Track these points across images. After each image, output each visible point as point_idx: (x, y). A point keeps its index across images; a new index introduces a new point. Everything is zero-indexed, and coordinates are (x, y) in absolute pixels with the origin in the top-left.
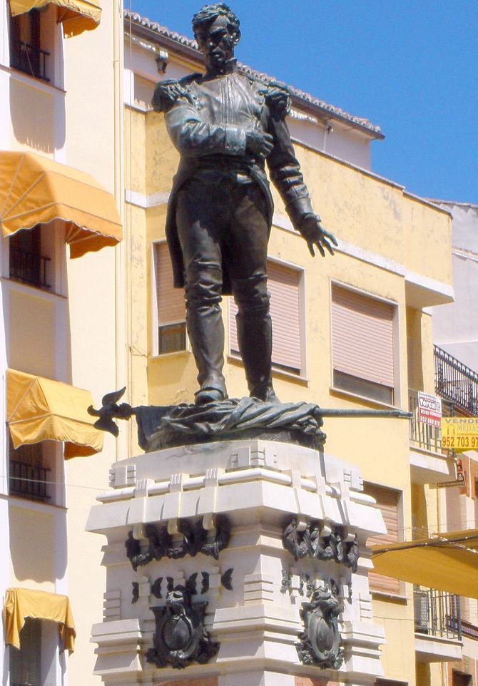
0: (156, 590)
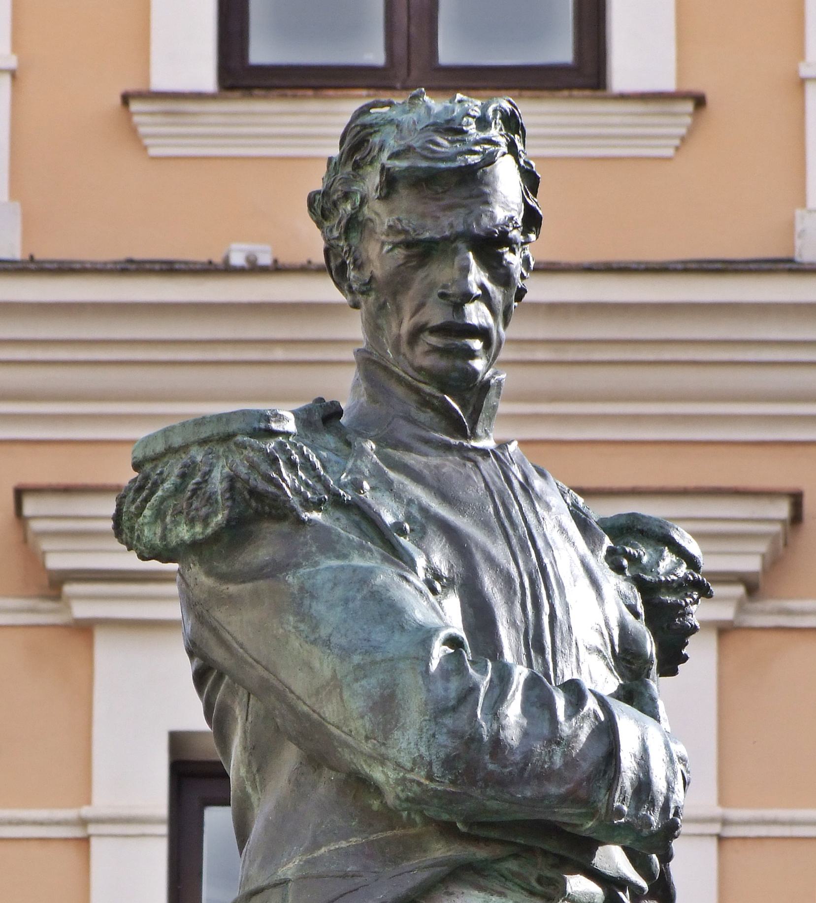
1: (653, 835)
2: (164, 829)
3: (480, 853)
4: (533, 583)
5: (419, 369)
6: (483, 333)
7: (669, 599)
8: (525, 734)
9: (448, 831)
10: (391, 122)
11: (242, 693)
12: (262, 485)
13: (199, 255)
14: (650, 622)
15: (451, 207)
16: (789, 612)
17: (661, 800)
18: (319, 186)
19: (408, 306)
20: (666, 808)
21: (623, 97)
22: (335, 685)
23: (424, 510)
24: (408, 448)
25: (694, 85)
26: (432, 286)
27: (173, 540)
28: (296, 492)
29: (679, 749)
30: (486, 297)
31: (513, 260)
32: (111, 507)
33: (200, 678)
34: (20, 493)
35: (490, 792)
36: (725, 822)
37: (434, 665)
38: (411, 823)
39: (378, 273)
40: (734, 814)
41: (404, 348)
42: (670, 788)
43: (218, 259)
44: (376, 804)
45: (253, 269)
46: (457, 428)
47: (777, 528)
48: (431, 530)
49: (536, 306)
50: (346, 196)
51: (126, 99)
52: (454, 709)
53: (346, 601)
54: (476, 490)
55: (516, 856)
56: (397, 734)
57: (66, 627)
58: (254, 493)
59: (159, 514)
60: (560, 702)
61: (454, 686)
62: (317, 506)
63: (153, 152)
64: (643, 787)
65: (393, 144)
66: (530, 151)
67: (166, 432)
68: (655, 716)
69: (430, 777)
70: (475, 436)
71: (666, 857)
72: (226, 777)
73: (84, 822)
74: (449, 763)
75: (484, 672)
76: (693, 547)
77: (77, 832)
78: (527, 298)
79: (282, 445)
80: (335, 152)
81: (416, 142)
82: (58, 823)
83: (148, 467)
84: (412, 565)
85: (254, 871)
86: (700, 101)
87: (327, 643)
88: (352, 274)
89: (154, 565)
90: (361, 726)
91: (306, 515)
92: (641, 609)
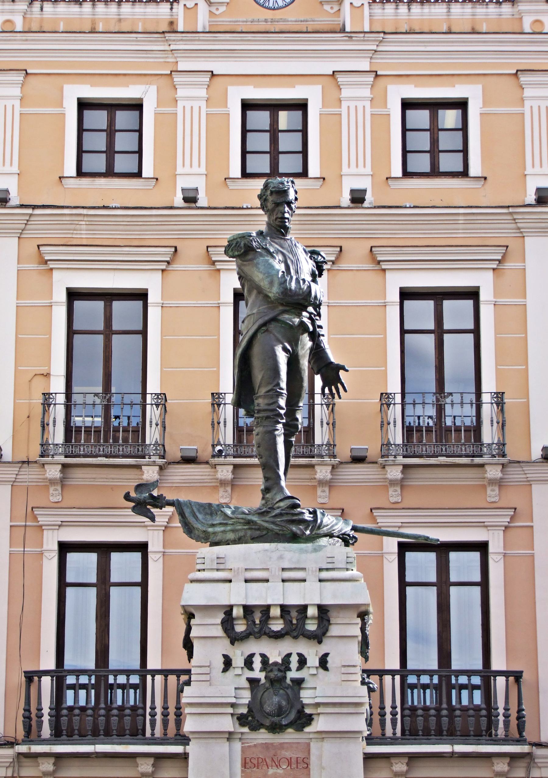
0: (249, 663)
1: (318, 305)
2: (233, 305)
3: (288, 308)
4: (297, 262)
5: (277, 225)
6: (288, 219)
7: (320, 264)
8: (295, 288)
9: (282, 305)
10: (272, 182)
11: (247, 281)
12: (250, 245)
13: (238, 206)
14: (317, 268)
15: (282, 197)
16: (340, 267)
17: (319, 299)
18: (259, 193)
19: (275, 214)
20: (320, 300)
21: (311, 178)
22: (263, 279)
23: (278, 249)
24: (275, 239)
25: (323, 176)
26: (279, 210)
27: (235, 254)
28: (256, 246)
29: (322, 290)
30: (288, 212)
31: (293, 206)
32: (223, 249)
33: (239, 278)
34: (208, 247)
35: (289, 298)
36: (329, 303)
37: (280, 276)
38: (275, 303)
39: (270, 208)
40: (330, 301)
41: (274, 221)
42: (320, 297)
43: (241, 207)
44: (270, 300)
45: (247, 208)
46: (284, 235)
47: (337, 252)
48: (279, 253)
49: (296, 214)
50: (264, 195)
51: (225, 179)
52: (283, 283)
53: (264, 265)
54: (286, 246)
55: (294, 309)
56: (273, 288)
57: (215, 270)
58: (249, 246)
59: (232, 250)
60: (301, 282)
61: (283, 279)
62: (259, 248)
63: (230, 188)
64: (316, 297)
65: (272, 186)
66: (296, 188)
67: (233, 236)
68: (317, 284)
69: (279, 295)
70: (286, 236)
71: (320, 309)
72: (244, 296)
73: (219, 304)
74: (282, 293)
75: (288, 277)
76: (324, 255)
77: (218, 305)
78: (295, 213)
79: (253, 238)
80: (262, 188)
81: (276, 186)
82: (214, 304)
83: (230, 242)
84: (275, 258)
85: (249, 311)
86: (324, 179)
87: (261, 272)
88: (265, 208)
89: (231, 259)
90: (267, 286)
91: (257, 250)
92: (315, 266)
